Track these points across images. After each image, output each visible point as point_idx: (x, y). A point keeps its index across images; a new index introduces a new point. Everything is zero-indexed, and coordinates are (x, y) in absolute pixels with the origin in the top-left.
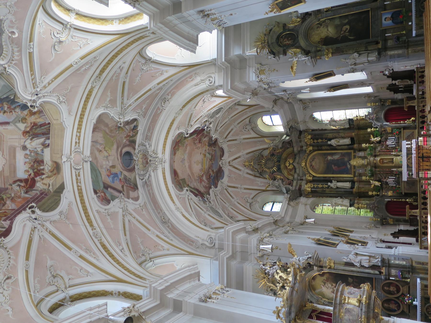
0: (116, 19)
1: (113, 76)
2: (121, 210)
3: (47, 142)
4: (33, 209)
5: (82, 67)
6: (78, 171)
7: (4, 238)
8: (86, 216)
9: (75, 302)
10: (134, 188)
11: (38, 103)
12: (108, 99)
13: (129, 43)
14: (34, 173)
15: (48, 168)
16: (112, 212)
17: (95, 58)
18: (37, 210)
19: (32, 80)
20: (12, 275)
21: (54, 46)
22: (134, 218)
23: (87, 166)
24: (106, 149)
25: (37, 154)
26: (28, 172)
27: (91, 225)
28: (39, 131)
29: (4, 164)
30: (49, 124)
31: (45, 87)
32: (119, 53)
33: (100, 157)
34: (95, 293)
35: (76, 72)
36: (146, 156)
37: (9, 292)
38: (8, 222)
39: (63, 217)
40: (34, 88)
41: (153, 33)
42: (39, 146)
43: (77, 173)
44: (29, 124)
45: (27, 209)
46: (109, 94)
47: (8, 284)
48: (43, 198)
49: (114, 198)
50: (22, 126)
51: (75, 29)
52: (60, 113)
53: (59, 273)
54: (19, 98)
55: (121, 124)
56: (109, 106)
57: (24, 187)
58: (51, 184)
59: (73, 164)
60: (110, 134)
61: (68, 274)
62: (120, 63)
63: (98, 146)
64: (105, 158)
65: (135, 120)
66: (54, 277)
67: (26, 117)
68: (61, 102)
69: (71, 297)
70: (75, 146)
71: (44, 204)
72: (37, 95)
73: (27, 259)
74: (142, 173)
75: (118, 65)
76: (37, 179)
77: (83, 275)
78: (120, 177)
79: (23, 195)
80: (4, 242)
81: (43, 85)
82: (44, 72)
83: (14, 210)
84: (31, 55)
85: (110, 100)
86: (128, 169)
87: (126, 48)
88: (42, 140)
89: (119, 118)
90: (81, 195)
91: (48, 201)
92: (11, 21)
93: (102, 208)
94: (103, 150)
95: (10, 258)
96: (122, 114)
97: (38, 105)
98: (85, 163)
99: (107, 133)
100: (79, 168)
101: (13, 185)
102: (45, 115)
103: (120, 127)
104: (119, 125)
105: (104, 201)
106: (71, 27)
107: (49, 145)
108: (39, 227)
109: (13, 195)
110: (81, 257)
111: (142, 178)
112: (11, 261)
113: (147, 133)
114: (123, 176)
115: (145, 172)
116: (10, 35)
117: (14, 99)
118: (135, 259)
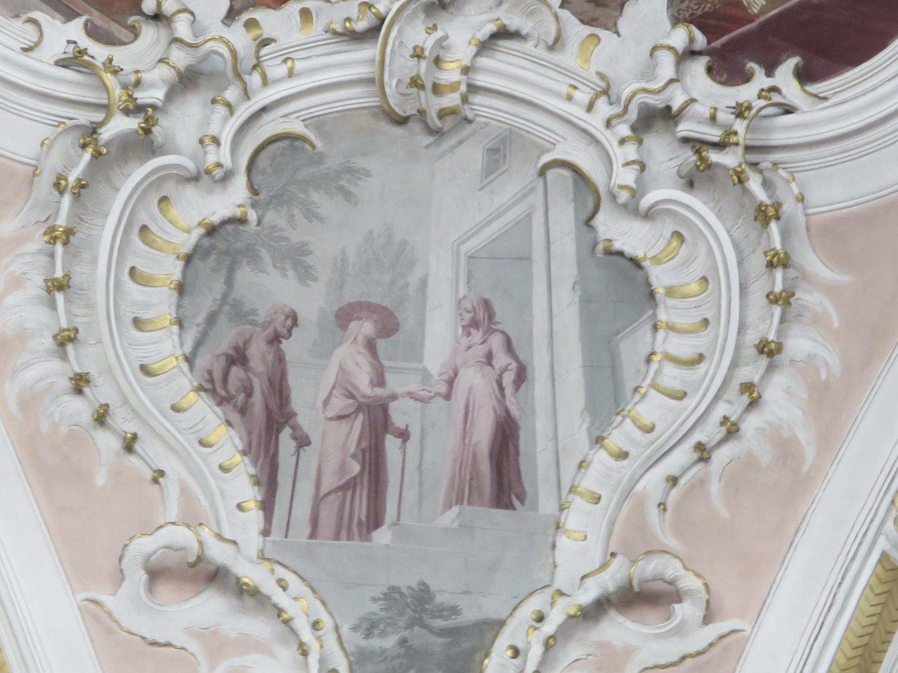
7: (805, 76)
20: (689, 582)
21: (557, 40)
80: (784, 129)
95: (769, 350)
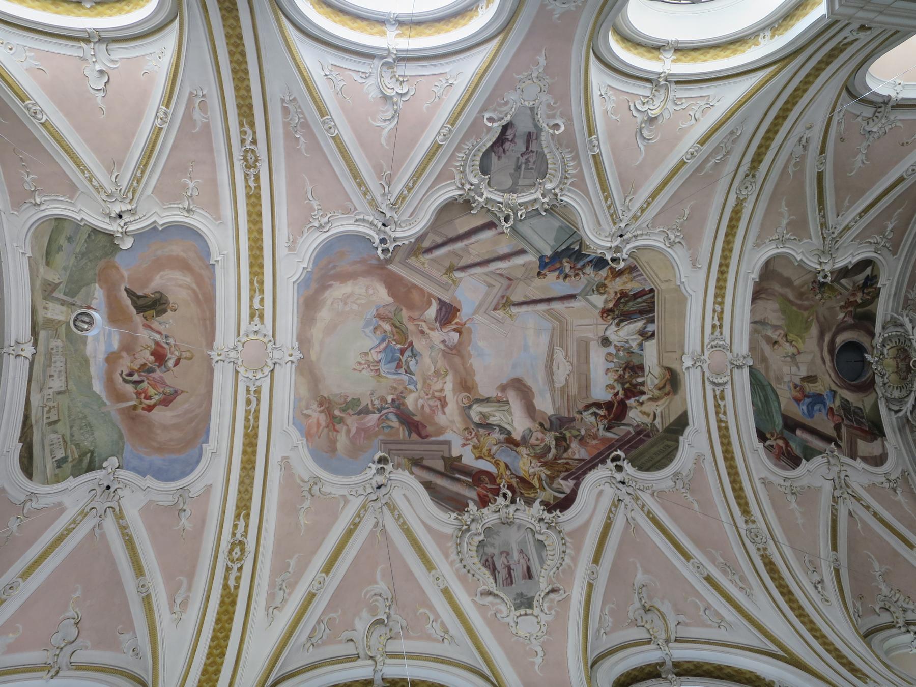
0: (763, 29)
1: (786, 167)
2: (828, 486)
3: (651, 328)
4: (618, 463)
5: (706, 160)
6: (721, 388)
7: (561, 512)
8: (734, 489)
9: (684, 679)
10: (873, 434)
11: (625, 251)
12: (784, 222)
13: (807, 76)
14: (624, 389)
15: (652, 382)
16: (802, 487)
17: (732, 133)
18: (626, 465)
19: (609, 207)
21: (641, 135)
22: (867, 508)
23: (743, 379)
24: (791, 337)
25: (630, 352)
26: (613, 388)
27: (746, 511)
28: (631, 306)
29: (568, 372)
30: (652, 290)
31: (635, 218)
32: (789, 106)
33: (776, 359)
34: (732, 672)
35: (697, 175)
36: (906, 350)
37: (549, 618)
38: (571, 483)
39: (680, 484)
40: (615, 224)
41: (862, 28)
42: (634, 337)
43: (718, 393)
44: (613, 295)
45: (609, 461)
46: (784, 209)
47: (552, 601)
48: (641, 441)
49: (810, 454)
50: (599, 300)
51: (677, 83)
52: (673, 267)
53: (658, 604)
54: (588, 247)
55: (826, 277)
56: (788, 236)
57: (604, 417)
58: (658, 414)
59: (707, 374)
60: (799, 302)
61: (678, 612)
62: (799, 129)
63: (769, 333)
64: (788, 359)
65: (866, 263)
66: (647, 611)
67: (606, 282)
68: (672, 245)
69: (676, 664)
70: (712, 334)
71: (641, 454)
72: (621, 236)
73: (596, 560)
74: (896, 394)
75: (793, 140)
76: (631, 402)
77: (710, 622)
78: (829, 404)
79: (602, 433)
80: (559, 520)
81: (631, 214)
82: (629, 187)
83: (583, 460)
84: (597, 159)
85: (788, 224)
86: (854, 386)
87: (805, 91)
88: (639, 325)
89: (821, 263)
90: (726, 441)
91: (653, 448)
92: (549, 106)
93: (778, 474)
94: (782, 341)
95: (564, 552)
96: (829, 248)
97: (625, 257)
98: (736, 371)
99: (790, 302)
100: (720, 381)
101: (585, 414)
102: (641, 275)
103: (824, 284)
104: (822, 280)
105: (782, 458)
106: (669, 82)
107: (653, 335)
108: (628, 499)
109: (583, 432)
110: (709, 579)
111: (896, 408)
112: (566, 558)
113: (907, 291)
114: (838, 402)
115: (904, 393)
116: (551, 131)
117: (580, 250)
118: (853, 618)
